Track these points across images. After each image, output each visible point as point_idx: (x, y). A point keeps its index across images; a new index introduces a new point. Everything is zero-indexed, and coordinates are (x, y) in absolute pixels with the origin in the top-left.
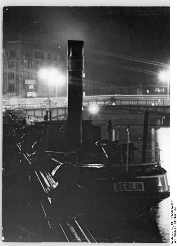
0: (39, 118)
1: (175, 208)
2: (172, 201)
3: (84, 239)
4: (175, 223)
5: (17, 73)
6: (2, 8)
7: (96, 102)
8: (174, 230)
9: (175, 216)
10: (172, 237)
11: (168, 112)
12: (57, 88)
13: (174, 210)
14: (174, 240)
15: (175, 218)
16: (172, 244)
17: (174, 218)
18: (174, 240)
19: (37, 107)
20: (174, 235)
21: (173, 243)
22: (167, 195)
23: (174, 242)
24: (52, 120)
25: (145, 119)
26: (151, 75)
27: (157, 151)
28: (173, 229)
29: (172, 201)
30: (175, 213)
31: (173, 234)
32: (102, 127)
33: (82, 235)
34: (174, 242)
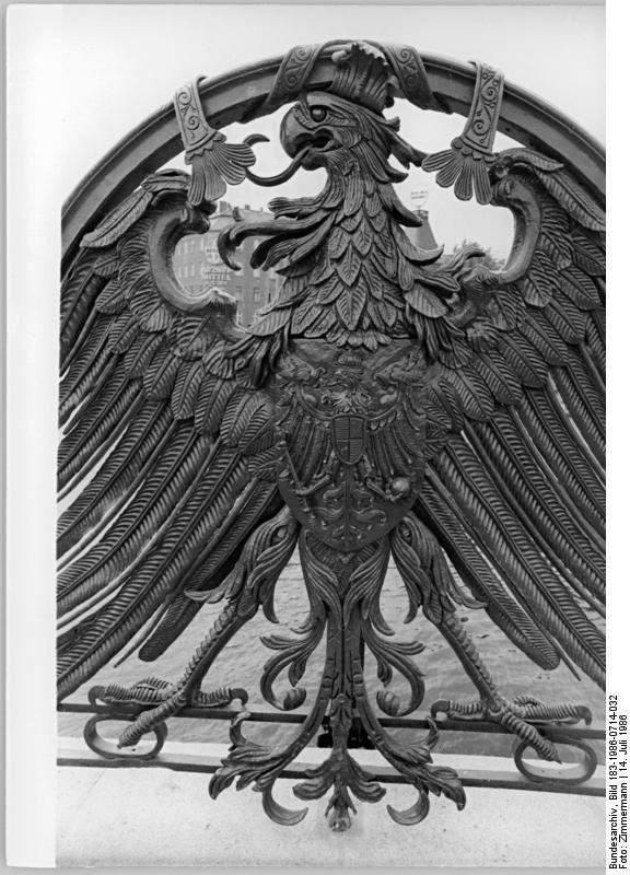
10: (614, 844)
14: (619, 854)
16: (613, 867)
18: (619, 854)
21: (617, 864)
23: (619, 859)
30: (623, 737)
31: (614, 832)
34: (619, 859)
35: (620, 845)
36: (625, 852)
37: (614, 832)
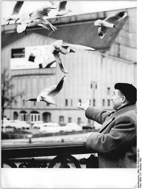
0: (58, 131)
1: (140, 159)
4: (141, 170)
5: (21, 132)
6: (9, 125)
8: (140, 176)
9: (141, 164)
13: (140, 160)
14: (140, 184)
15: (141, 166)
16: (138, 187)
17: (140, 167)
18: (140, 184)
19: (128, 107)
20: (139, 181)
21: (139, 187)
22: (132, 84)
23: (140, 186)
26: (131, 133)
28: (139, 176)
30: (141, 163)
33: (48, 165)
34: (140, 186)
35: (140, 182)
36: (141, 177)
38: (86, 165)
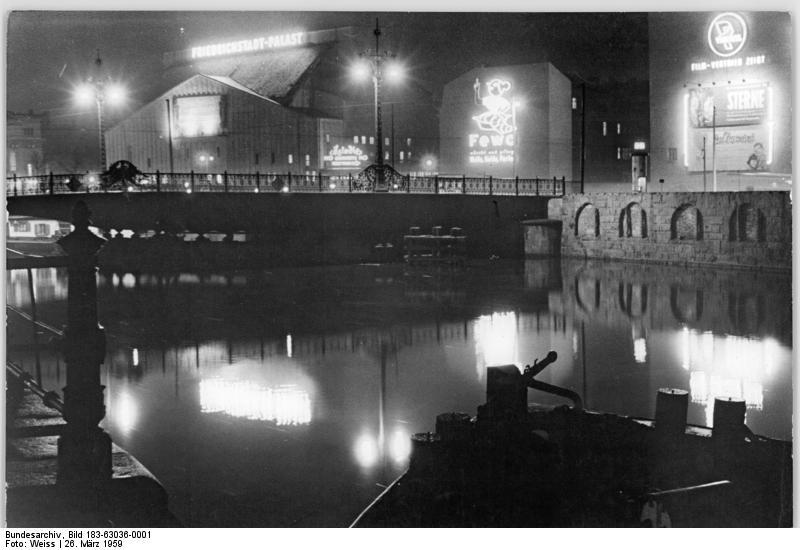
2: (147, 535)
3: (10, 369)
7: (691, 94)
10: (28, 535)
11: (649, 511)
12: (100, 120)
14: (19, 540)
16: (8, 534)
18: (19, 540)
20: (35, 539)
21: (10, 539)
23: (14, 540)
24: (494, 194)
25: (554, 393)
27: (628, 180)
29: (147, 535)
30: (102, 544)
31: (39, 536)
32: (564, 223)
34: (14, 540)
36: (21, 545)
37: (39, 536)
38: (100, 425)
